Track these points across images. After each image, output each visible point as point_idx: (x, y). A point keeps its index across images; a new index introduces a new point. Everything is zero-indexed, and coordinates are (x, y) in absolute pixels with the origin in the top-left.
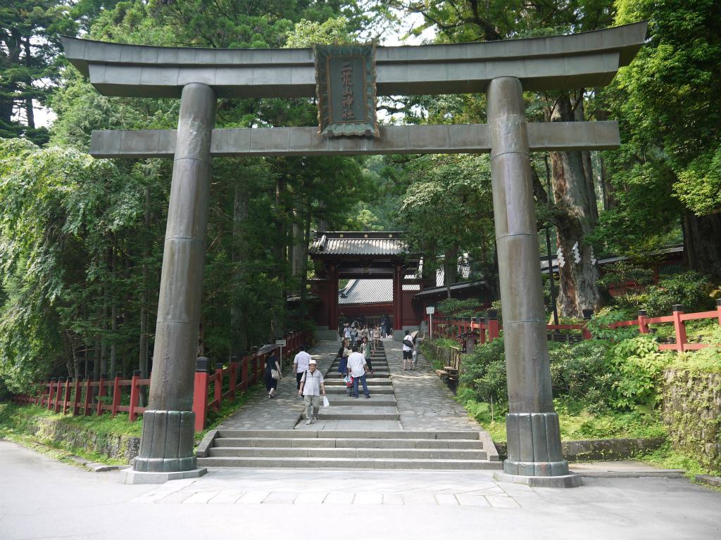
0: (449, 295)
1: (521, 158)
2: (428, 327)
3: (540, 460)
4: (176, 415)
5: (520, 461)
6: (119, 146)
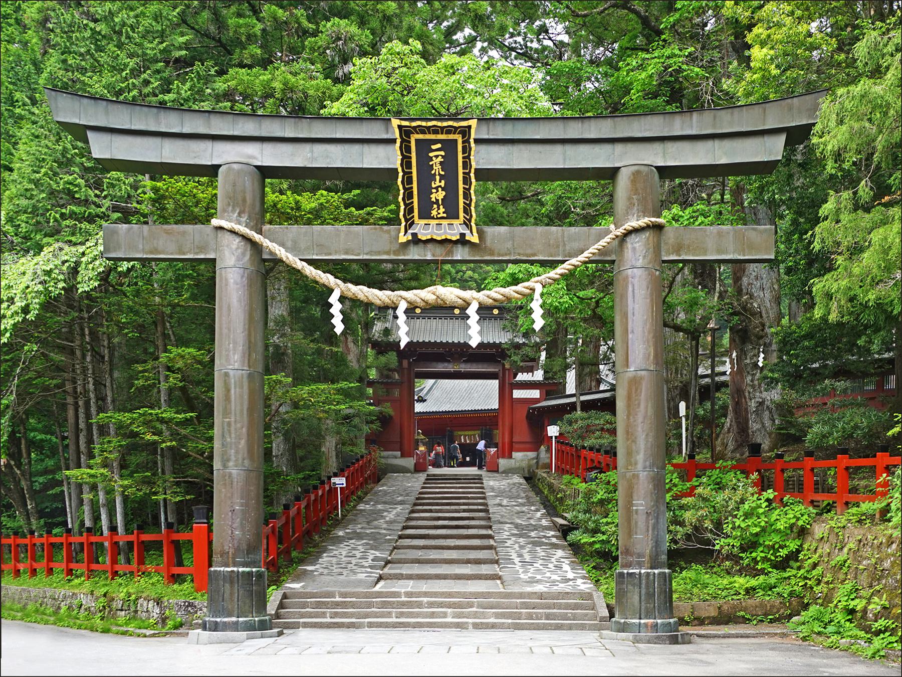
0: (579, 408)
1: (651, 275)
2: (549, 455)
3: (646, 618)
4: (248, 573)
5: (640, 619)
6: (141, 246)
